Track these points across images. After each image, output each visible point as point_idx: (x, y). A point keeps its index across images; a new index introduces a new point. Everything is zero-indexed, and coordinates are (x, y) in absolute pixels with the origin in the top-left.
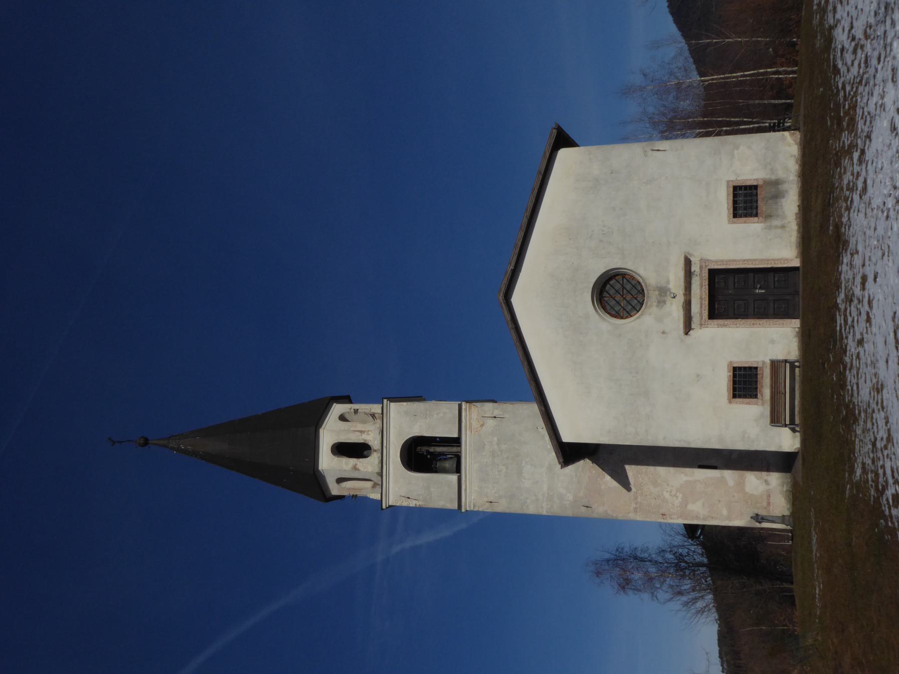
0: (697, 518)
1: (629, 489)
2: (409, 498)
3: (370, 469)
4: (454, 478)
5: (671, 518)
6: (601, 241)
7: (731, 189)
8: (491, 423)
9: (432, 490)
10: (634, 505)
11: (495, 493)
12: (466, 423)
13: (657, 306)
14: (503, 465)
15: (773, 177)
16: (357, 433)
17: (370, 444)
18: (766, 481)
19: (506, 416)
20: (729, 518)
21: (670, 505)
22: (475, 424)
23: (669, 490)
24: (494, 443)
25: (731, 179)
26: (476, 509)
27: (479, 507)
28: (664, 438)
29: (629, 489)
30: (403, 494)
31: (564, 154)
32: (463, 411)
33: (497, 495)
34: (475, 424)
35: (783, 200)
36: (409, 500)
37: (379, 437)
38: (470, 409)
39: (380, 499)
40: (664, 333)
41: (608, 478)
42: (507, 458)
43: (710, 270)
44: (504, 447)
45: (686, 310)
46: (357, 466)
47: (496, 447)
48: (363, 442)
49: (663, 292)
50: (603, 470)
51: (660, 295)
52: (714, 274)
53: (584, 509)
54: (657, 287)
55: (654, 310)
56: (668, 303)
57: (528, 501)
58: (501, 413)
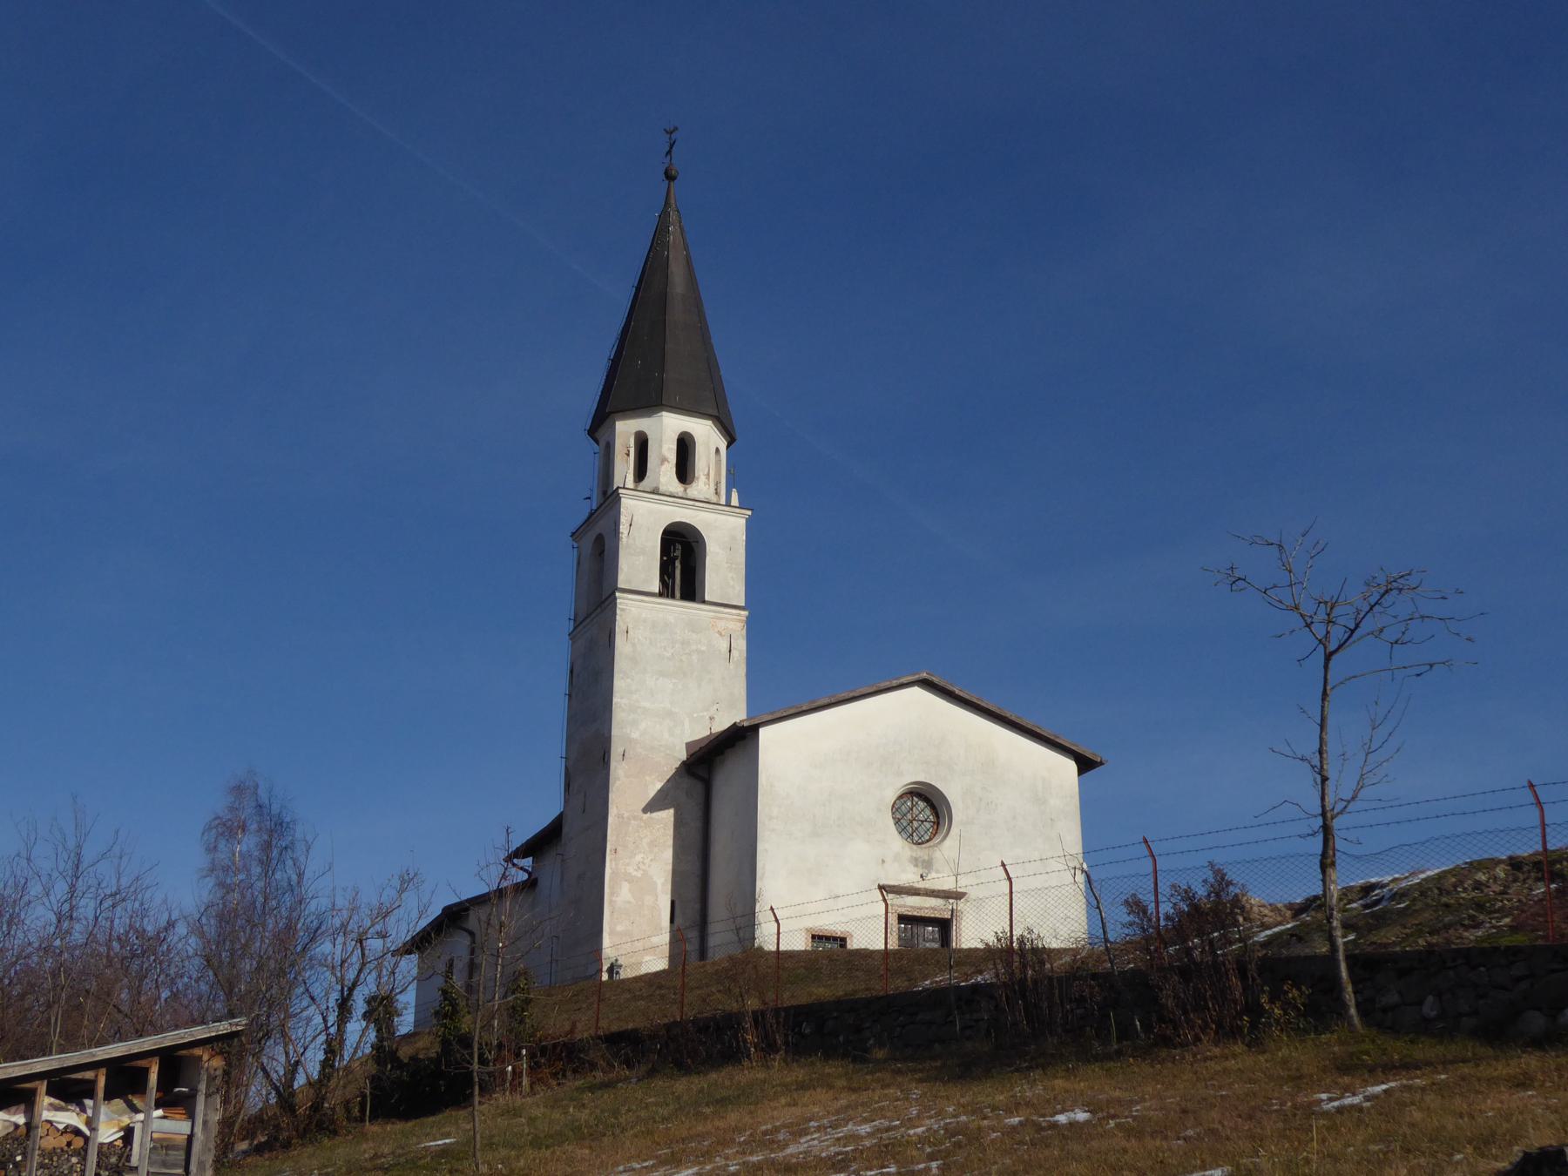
0: (612, 894)
1: (645, 810)
3: (663, 480)
4: (656, 590)
6: (981, 800)
8: (724, 645)
9: (642, 558)
10: (626, 815)
11: (639, 640)
12: (723, 613)
16: (707, 470)
17: (694, 484)
20: (612, 933)
21: (627, 861)
22: (721, 625)
23: (645, 861)
24: (699, 646)
26: (618, 612)
27: (621, 616)
29: (645, 810)
31: (1071, 766)
32: (734, 611)
33: (636, 640)
34: (721, 625)
36: (628, 525)
37: (701, 497)
38: (739, 621)
39: (732, 504)
40: (883, 861)
41: (659, 786)
42: (681, 660)
44: (695, 657)
45: (910, 890)
47: (694, 647)
49: (928, 865)
50: (668, 781)
51: (924, 861)
53: (621, 750)
54: (932, 859)
57: (629, 680)
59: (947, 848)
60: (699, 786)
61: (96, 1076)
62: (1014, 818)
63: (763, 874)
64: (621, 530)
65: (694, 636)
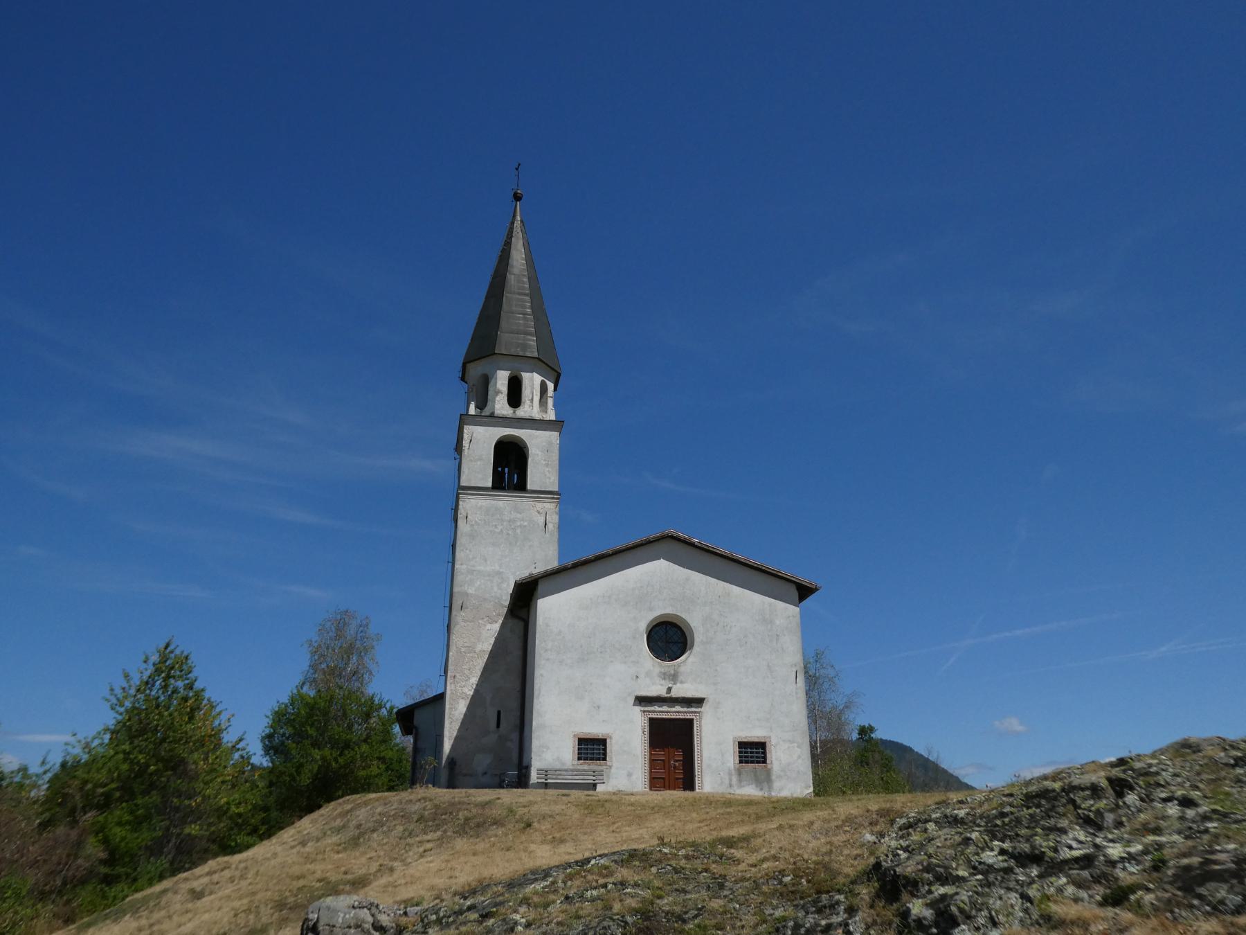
2: (471, 441)
4: (490, 484)
5: (451, 684)
7: (763, 741)
8: (541, 520)
9: (479, 463)
13: (661, 672)
14: (501, 530)
15: (773, 777)
16: (531, 396)
17: (521, 407)
18: (485, 773)
19: (547, 535)
24: (522, 522)
25: (772, 740)
28: (542, 675)
30: (474, 435)
35: (754, 786)
40: (637, 677)
42: (508, 534)
43: (693, 719)
44: (518, 531)
46: (500, 395)
47: (519, 524)
48: (523, 400)
49: (674, 677)
51: (671, 675)
52: (690, 723)
55: (657, 670)
56: (663, 682)
58: (550, 530)
59: (688, 662)
60: (521, 624)
61: (541, 493)
62: (746, 636)
63: (539, 694)
64: (464, 445)
65: (519, 516)
